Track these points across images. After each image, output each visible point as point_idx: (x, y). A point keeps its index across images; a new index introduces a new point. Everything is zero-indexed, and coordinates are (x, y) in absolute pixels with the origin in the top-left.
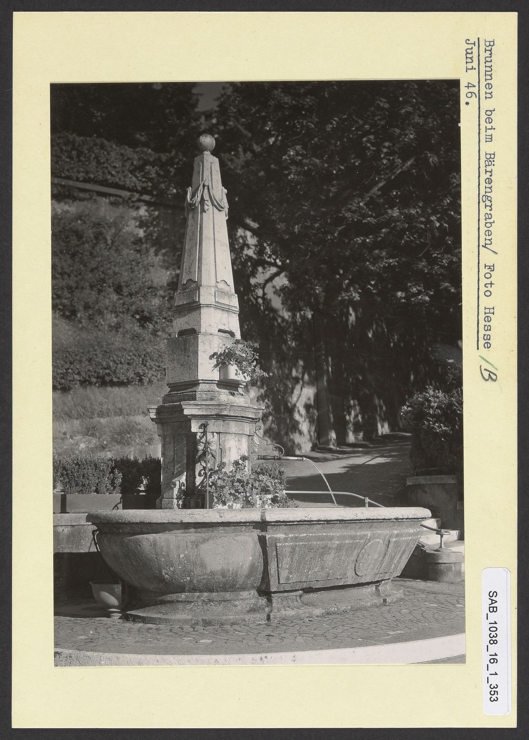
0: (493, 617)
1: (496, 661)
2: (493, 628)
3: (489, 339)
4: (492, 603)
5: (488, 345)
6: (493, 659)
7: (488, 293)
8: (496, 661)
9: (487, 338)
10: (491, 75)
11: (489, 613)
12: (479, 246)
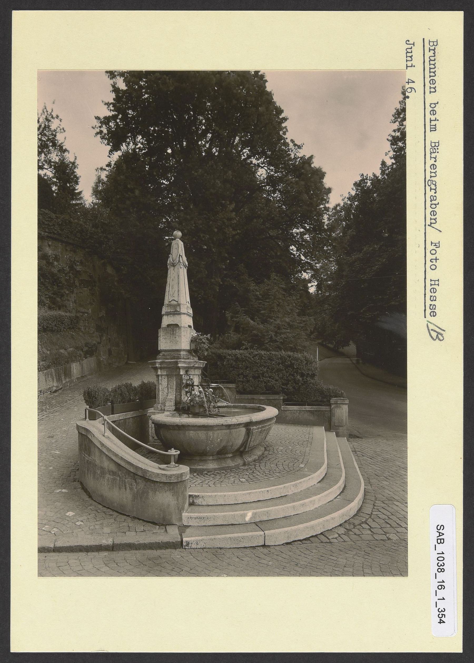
0: (440, 548)
1: (443, 587)
2: (441, 558)
3: (435, 309)
4: (440, 536)
5: (433, 314)
6: (441, 585)
7: (433, 267)
8: (443, 587)
9: (433, 307)
10: (434, 72)
11: (437, 544)
12: (425, 225)
